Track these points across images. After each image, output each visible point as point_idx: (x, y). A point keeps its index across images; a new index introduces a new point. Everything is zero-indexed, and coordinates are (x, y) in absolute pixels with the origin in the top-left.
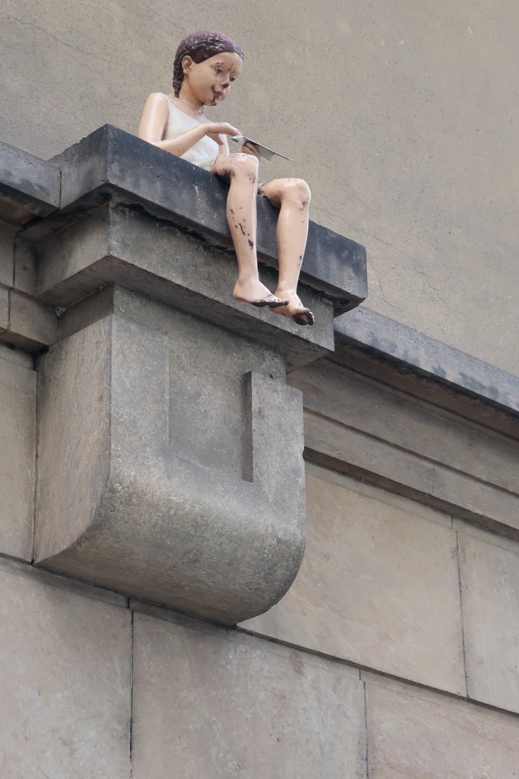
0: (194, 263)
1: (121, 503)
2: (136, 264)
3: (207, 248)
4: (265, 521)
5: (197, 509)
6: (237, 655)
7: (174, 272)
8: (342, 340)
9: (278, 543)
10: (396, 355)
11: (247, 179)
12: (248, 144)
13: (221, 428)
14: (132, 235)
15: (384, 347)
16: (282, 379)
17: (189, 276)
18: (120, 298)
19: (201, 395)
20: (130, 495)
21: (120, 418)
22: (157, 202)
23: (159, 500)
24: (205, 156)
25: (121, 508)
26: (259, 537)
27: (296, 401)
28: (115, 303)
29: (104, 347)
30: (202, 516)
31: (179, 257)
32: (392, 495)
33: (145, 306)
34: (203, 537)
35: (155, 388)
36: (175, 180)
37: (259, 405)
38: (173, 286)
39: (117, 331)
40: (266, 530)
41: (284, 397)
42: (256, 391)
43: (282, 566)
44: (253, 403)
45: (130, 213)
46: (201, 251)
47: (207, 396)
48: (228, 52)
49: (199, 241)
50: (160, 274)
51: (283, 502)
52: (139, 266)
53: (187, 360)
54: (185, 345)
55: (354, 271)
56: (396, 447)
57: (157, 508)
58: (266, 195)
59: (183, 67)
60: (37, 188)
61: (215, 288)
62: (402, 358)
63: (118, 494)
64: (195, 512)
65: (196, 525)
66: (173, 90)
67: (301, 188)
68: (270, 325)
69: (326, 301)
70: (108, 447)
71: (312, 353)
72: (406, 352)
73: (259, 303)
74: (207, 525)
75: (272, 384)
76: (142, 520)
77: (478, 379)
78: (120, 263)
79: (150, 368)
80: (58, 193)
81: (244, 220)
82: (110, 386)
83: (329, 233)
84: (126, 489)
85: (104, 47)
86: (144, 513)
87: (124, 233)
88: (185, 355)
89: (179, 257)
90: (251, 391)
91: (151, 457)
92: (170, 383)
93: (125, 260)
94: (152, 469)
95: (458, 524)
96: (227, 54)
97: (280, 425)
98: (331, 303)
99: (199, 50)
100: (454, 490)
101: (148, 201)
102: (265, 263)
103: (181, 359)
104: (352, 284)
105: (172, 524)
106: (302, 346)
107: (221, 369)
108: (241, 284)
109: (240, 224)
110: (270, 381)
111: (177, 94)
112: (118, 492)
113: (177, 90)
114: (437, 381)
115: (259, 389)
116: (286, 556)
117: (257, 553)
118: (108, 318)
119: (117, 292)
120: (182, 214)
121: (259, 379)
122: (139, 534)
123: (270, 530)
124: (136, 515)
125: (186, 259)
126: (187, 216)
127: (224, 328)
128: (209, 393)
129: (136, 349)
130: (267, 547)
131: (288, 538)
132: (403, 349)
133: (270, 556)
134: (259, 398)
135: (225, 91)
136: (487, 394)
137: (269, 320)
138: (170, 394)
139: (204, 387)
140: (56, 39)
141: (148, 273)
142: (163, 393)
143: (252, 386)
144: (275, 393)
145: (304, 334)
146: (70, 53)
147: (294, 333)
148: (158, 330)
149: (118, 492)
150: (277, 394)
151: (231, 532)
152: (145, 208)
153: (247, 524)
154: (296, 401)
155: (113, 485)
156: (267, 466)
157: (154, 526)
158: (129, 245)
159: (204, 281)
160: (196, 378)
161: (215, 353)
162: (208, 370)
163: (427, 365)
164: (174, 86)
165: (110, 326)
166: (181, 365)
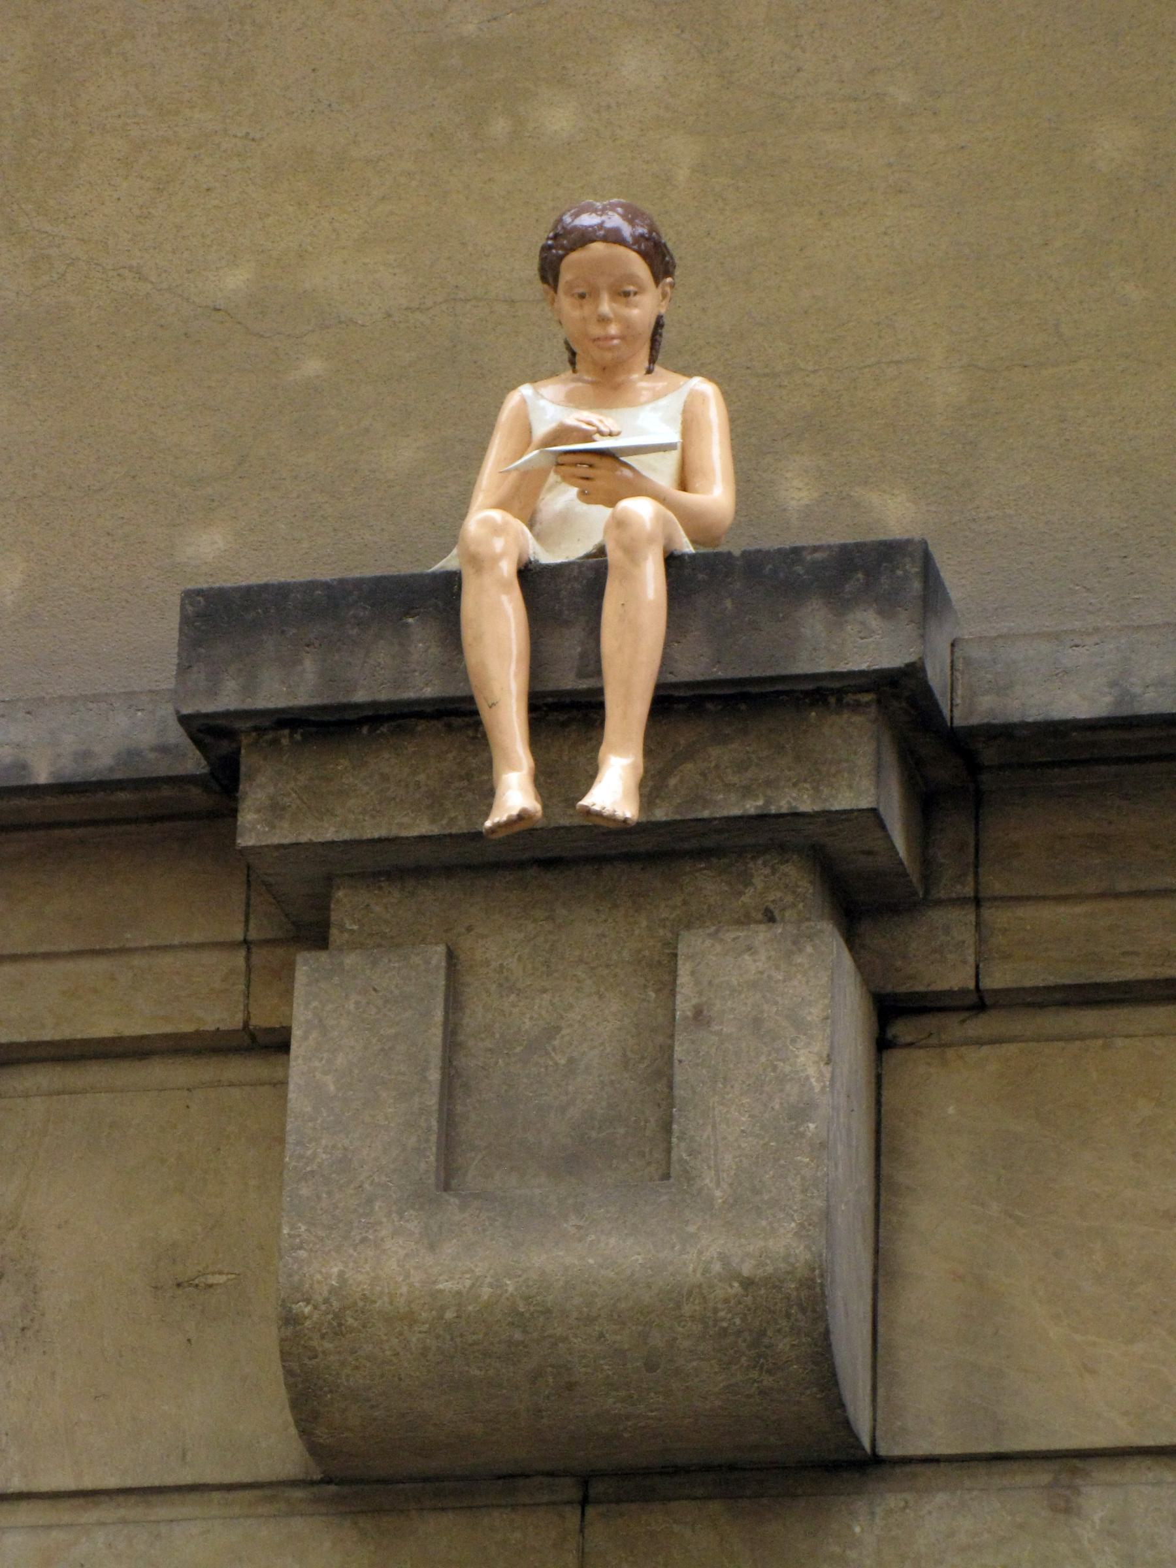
1: (323, 1337)
4: (700, 1253)
5: (511, 1289)
6: (877, 1520)
9: (746, 1289)
13: (612, 1082)
18: (347, 908)
20: (336, 1316)
21: (307, 1164)
23: (410, 1302)
25: (327, 1345)
26: (690, 1293)
27: (809, 949)
30: (527, 1299)
34: (550, 1336)
37: (694, 1001)
40: (706, 1271)
41: (773, 953)
43: (779, 1331)
54: (521, 936)
57: (410, 1318)
63: (308, 1323)
64: (507, 1295)
74: (548, 1311)
75: (738, 937)
76: (388, 1353)
84: (323, 1307)
86: (385, 1338)
88: (520, 959)
91: (384, 1220)
98: (866, 698)
103: (508, 969)
105: (462, 1336)
112: (306, 1318)
116: (778, 1308)
117: (700, 1326)
122: (400, 1379)
123: (717, 1267)
124: (368, 1348)
130: (719, 1306)
131: (770, 1269)
133: (738, 1321)
134: (697, 983)
144: (746, 957)
149: (306, 1318)
151: (614, 1305)
153: (652, 1276)
154: (809, 949)
155: (290, 1310)
156: (714, 1127)
157: (422, 1354)
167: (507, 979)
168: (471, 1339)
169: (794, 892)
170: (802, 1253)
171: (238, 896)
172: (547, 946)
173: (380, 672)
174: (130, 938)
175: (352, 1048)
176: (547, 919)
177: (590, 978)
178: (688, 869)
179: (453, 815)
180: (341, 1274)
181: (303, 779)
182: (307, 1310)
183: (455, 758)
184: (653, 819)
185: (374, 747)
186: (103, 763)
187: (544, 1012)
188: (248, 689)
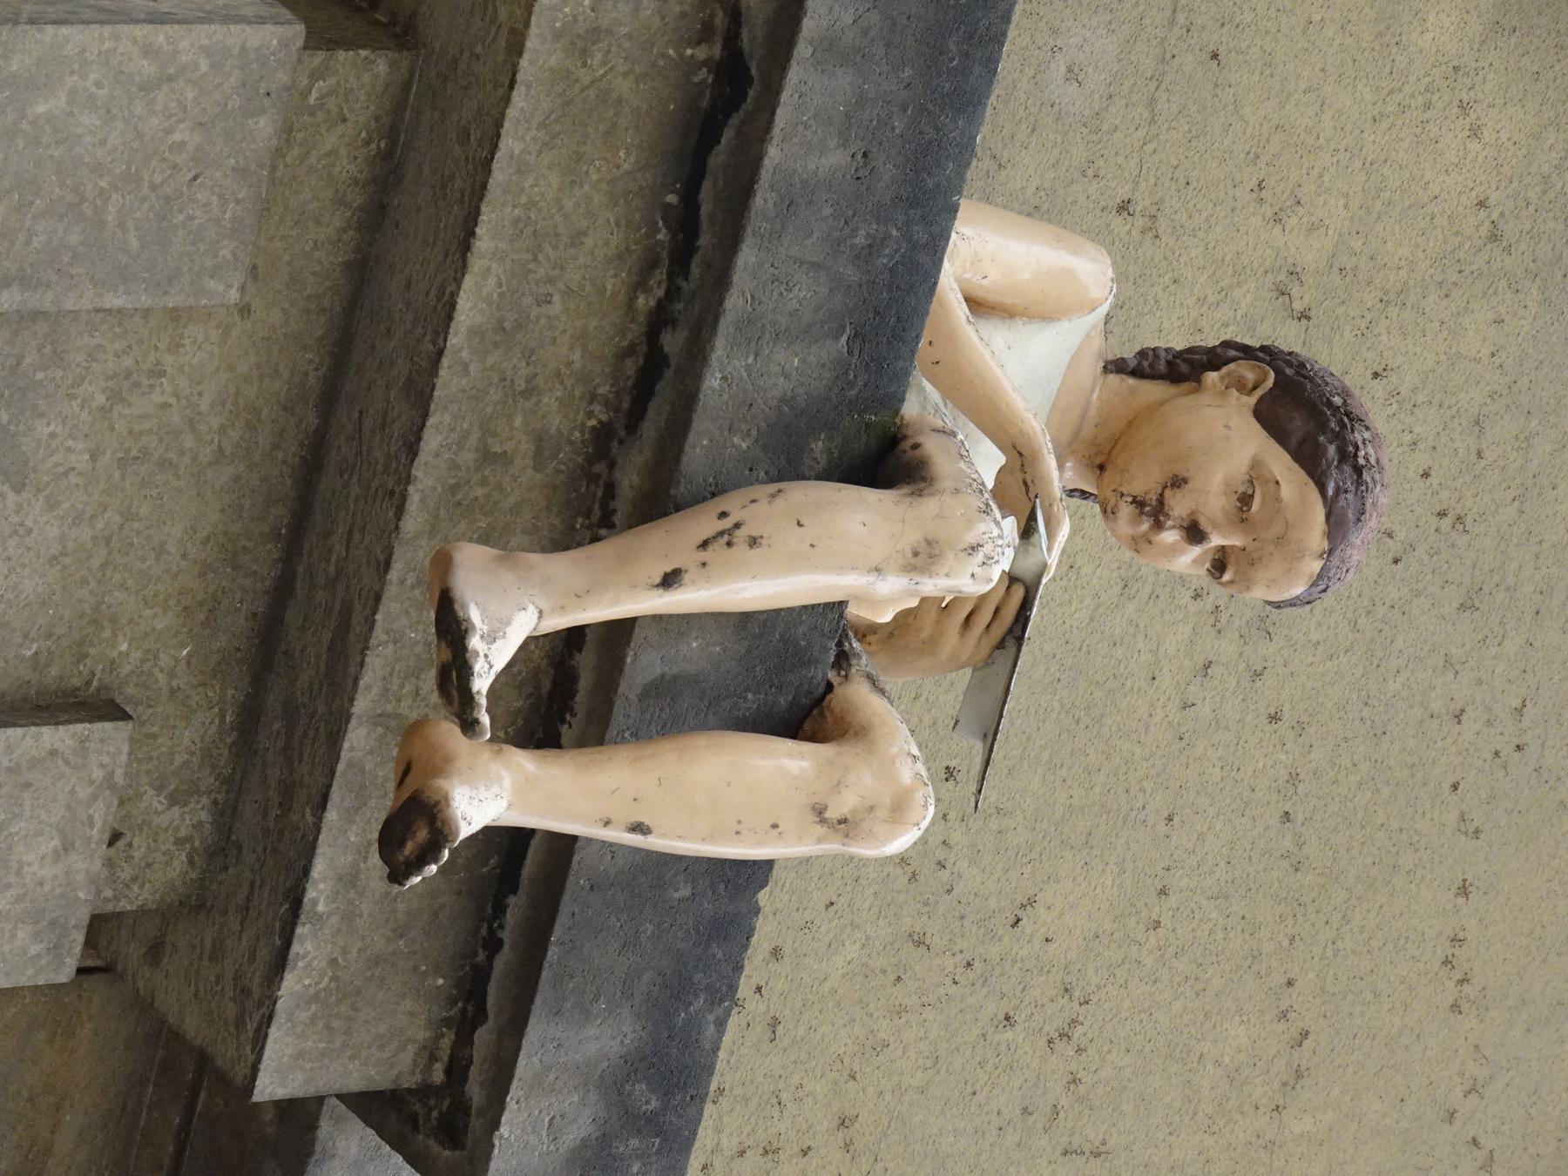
0: (540, 381)
3: (603, 443)
7: (500, 285)
11: (912, 537)
12: (1018, 593)
14: (626, 74)
16: (108, 893)
17: (490, 360)
18: (362, 76)
19: (18, 491)
22: (774, 154)
28: (342, 55)
31: (557, 307)
33: (340, 202)
35: (37, 242)
36: (860, 240)
38: (442, 290)
39: (243, 48)
41: (47, 887)
42: (58, 744)
45: (704, 63)
46: (590, 415)
47: (15, 519)
48: (1328, 516)
49: (626, 405)
50: (489, 217)
52: (511, 113)
53: (147, 417)
54: (204, 406)
55: (584, 1144)
58: (838, 691)
59: (1225, 370)
61: (454, 489)
66: (1129, 353)
68: (332, 773)
69: (446, 1043)
71: (230, 1010)
73: (452, 611)
75: (92, 826)
78: (513, 31)
81: (753, 542)
82: (32, 22)
83: (719, 1012)
85: (1182, 181)
87: (629, 37)
88: (165, 406)
89: (557, 307)
90: (57, 724)
93: (528, 44)
98: (438, 1075)
99: (1308, 416)
101: (773, 113)
102: (574, 715)
103: (151, 386)
104: (532, 1139)
106: (252, 958)
107: (122, 586)
109: (737, 526)
111: (1116, 366)
113: (1133, 364)
115: (67, 762)
120: (735, 278)
121: (105, 760)
125: (554, 341)
126: (734, 302)
127: (282, 591)
128: (29, 532)
129: (183, 144)
134: (34, 763)
135: (1171, 536)
137: (350, 765)
139: (52, 505)
141: (487, 165)
143: (79, 727)
144: (56, 842)
145: (309, 946)
146: (1147, 21)
147: (311, 894)
148: (255, 267)
150: (55, 851)
152: (735, 120)
154: (35, 949)
158: (585, 65)
159: (476, 435)
160: (81, 461)
161: (184, 556)
162: (117, 518)
164: (1142, 354)
166: (125, 385)
167: (137, 385)
169: (134, 879)
172: (172, 456)
175: (103, 143)
176: (220, 449)
177: (94, 538)
178: (231, 692)
179: (472, 368)
181: (623, 86)
183: (570, 364)
184: (353, 723)
185: (638, 216)
187: (57, 458)
188: (832, 51)
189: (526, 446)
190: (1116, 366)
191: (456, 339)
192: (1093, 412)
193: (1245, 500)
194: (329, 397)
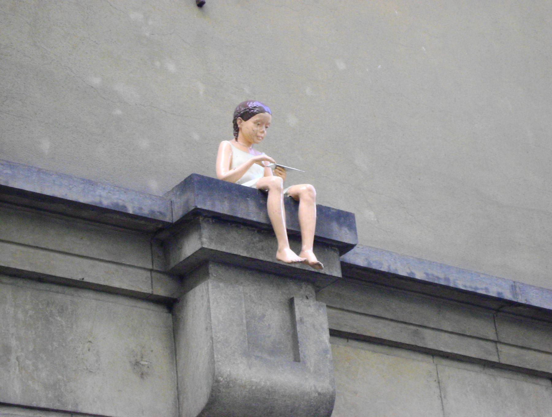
2: (219, 249)
8: (346, 267)
10: (382, 269)
12: (278, 167)
15: (375, 266)
18: (212, 269)
20: (228, 383)
24: (254, 179)
25: (224, 390)
29: (206, 299)
32: (394, 349)
44: (296, 315)
51: (320, 370)
56: (392, 320)
57: (244, 387)
60: (158, 214)
62: (386, 271)
63: (221, 383)
65: (269, 393)
66: (234, 137)
67: (310, 190)
70: (212, 356)
72: (389, 267)
74: (275, 392)
77: (436, 274)
79: (233, 307)
80: (171, 214)
89: (243, 240)
92: (246, 312)
94: (240, 365)
95: (437, 360)
96: (261, 114)
97: (314, 326)
100: (431, 340)
108: (279, 252)
110: (306, 301)
111: (236, 139)
114: (411, 280)
118: (206, 281)
119: (211, 265)
123: (313, 388)
132: (387, 265)
136: (443, 283)
138: (246, 318)
139: (267, 310)
140: (165, 112)
142: (242, 319)
160: (261, 306)
163: (403, 272)
165: (208, 286)
168: (257, 395)
170: (331, 389)
171: (149, 257)
173: (248, 211)
174: (123, 261)
180: (230, 372)
182: (222, 379)
186: (146, 212)
188: (213, 205)
189: (260, 244)
190: (236, 139)
191: (248, 256)
192: (244, 144)
193: (258, 124)
194: (251, 269)
